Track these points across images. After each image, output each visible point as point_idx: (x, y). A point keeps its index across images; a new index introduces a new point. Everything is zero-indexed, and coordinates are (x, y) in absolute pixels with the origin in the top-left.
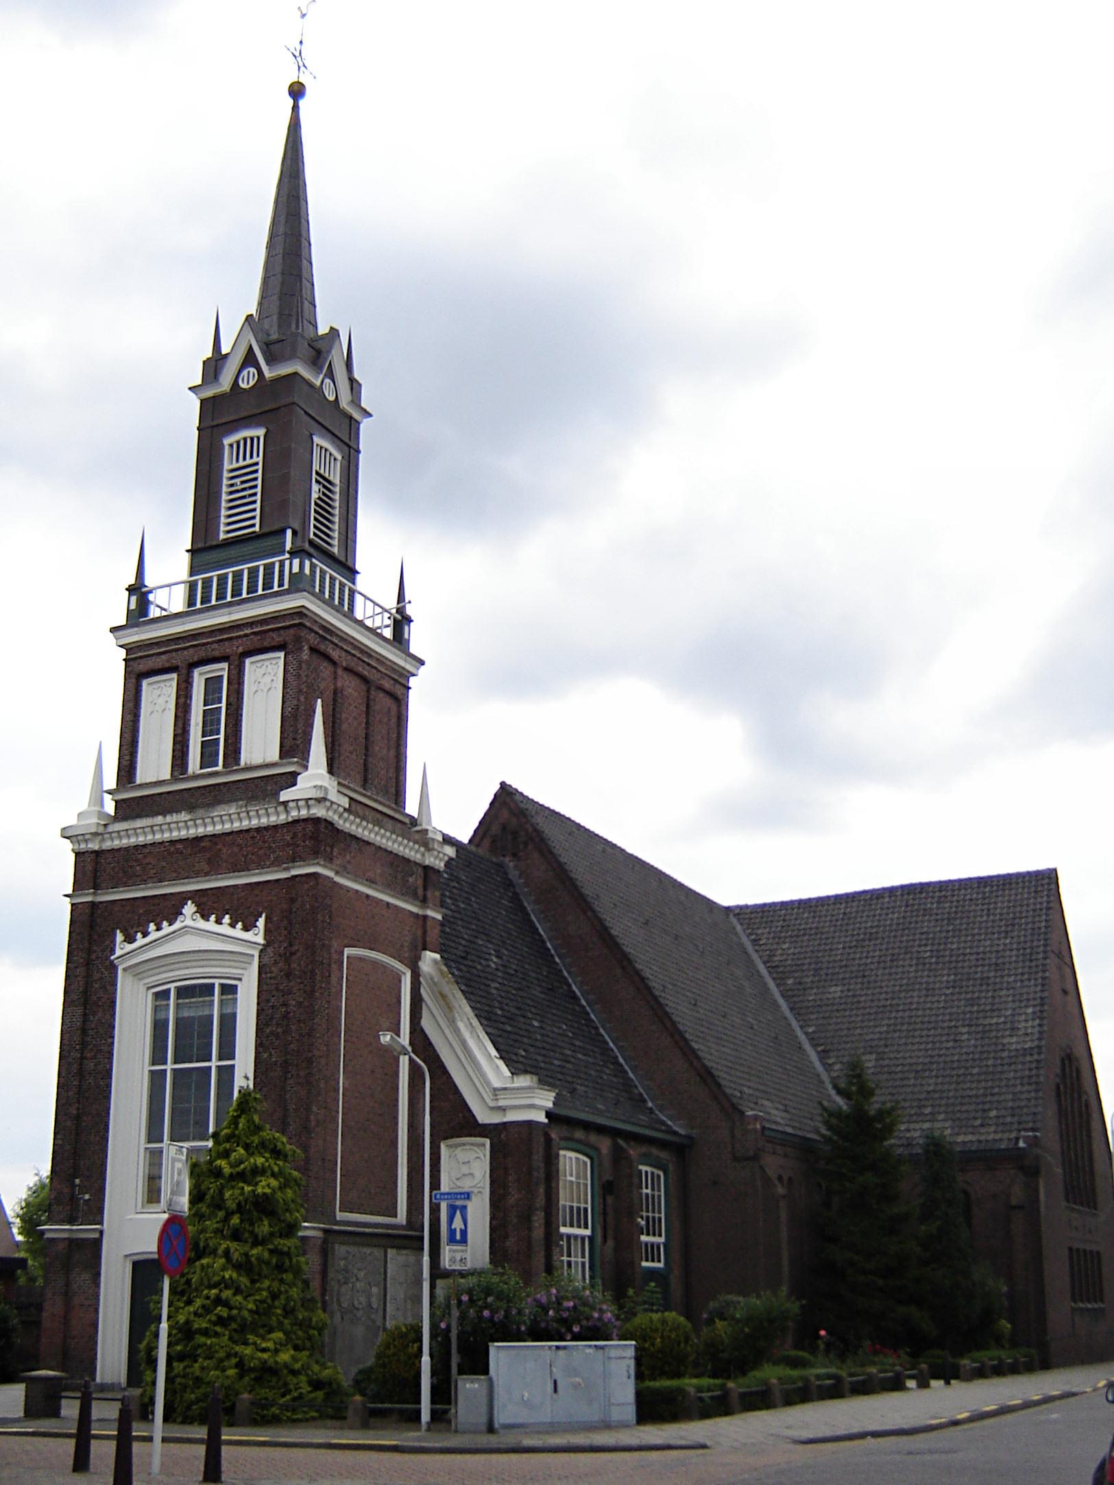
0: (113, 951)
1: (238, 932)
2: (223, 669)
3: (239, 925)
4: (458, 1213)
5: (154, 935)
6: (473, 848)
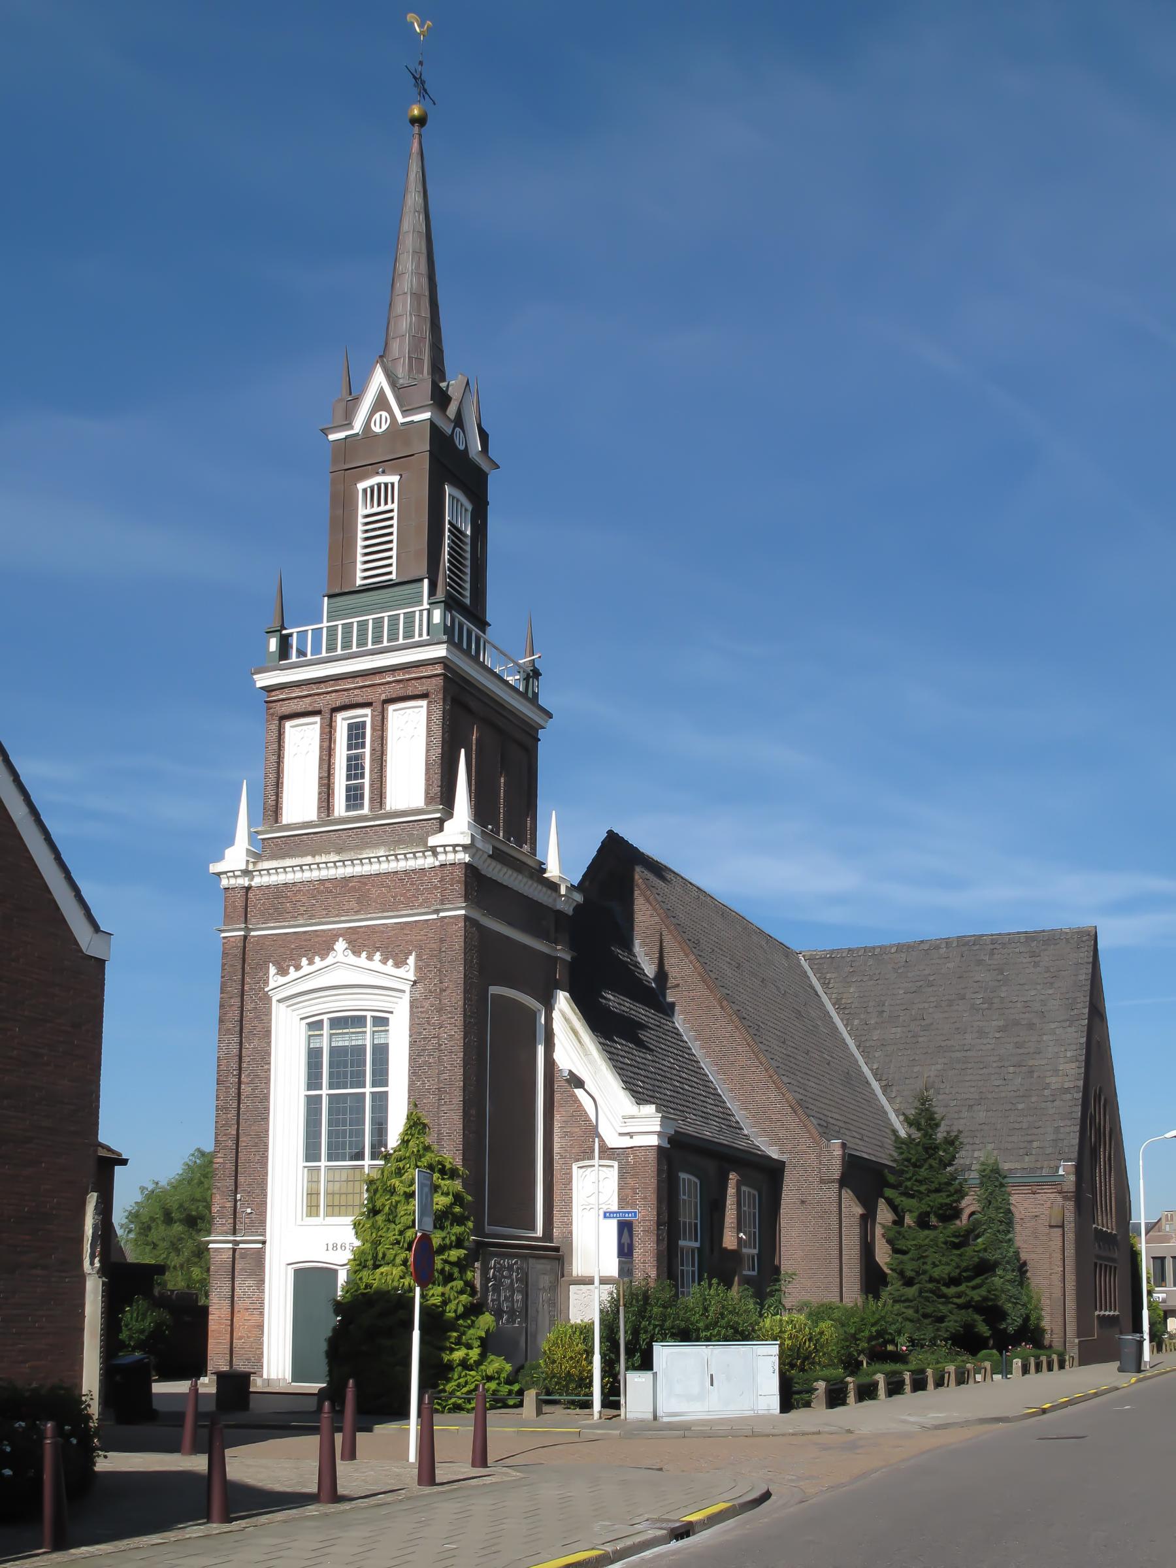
0: (266, 983)
1: (389, 967)
2: (366, 716)
3: (390, 962)
4: (626, 1230)
5: (306, 968)
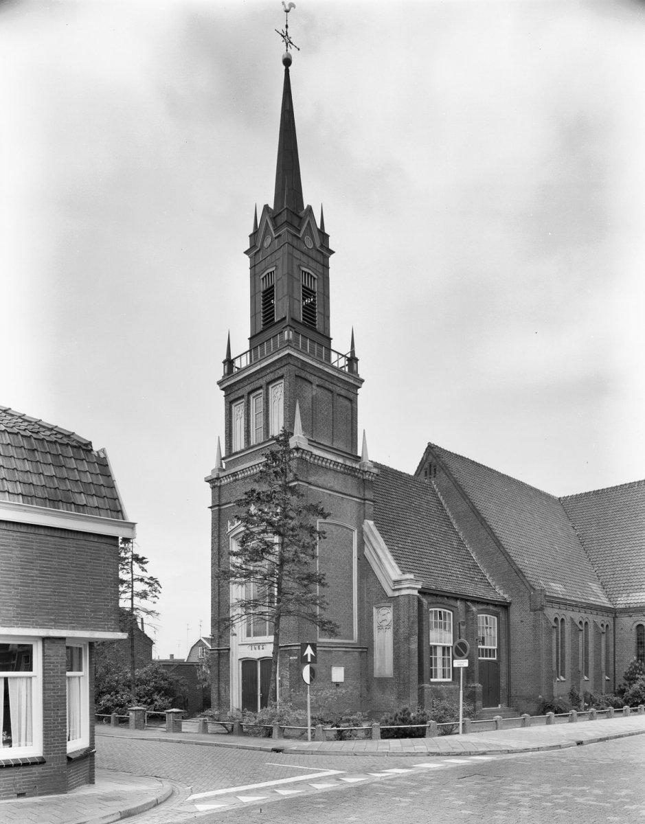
6: (422, 478)
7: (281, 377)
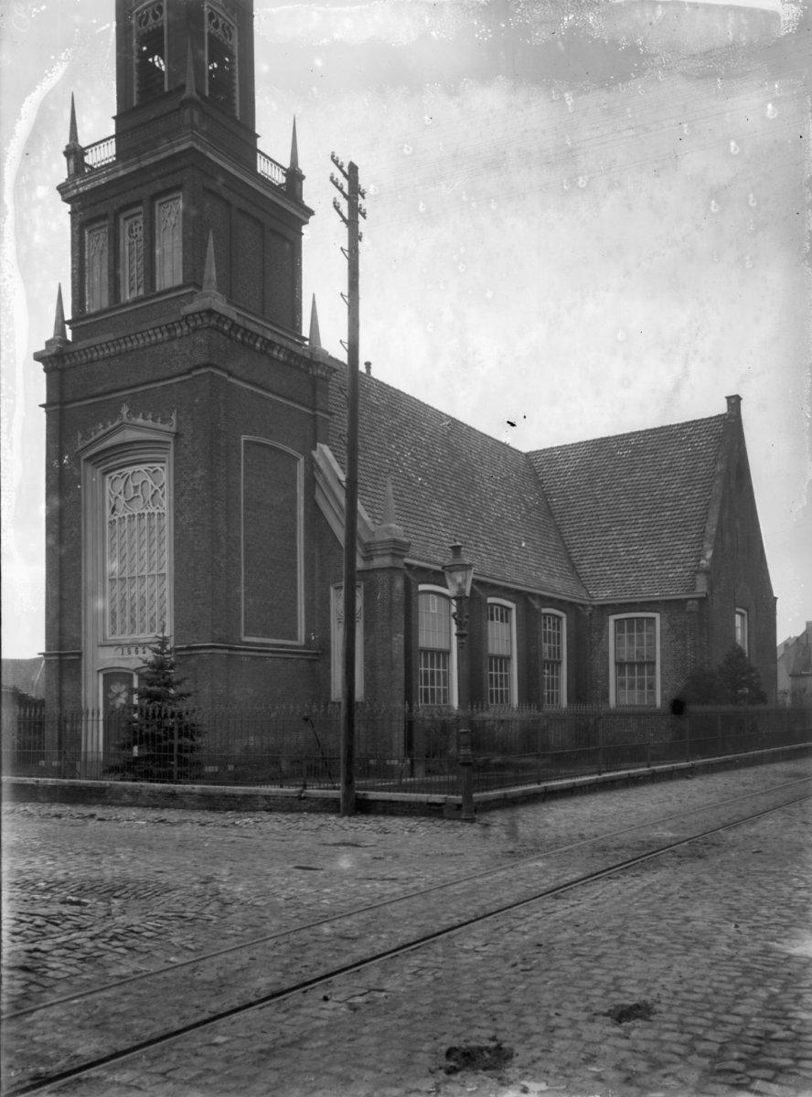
7: (179, 188)
